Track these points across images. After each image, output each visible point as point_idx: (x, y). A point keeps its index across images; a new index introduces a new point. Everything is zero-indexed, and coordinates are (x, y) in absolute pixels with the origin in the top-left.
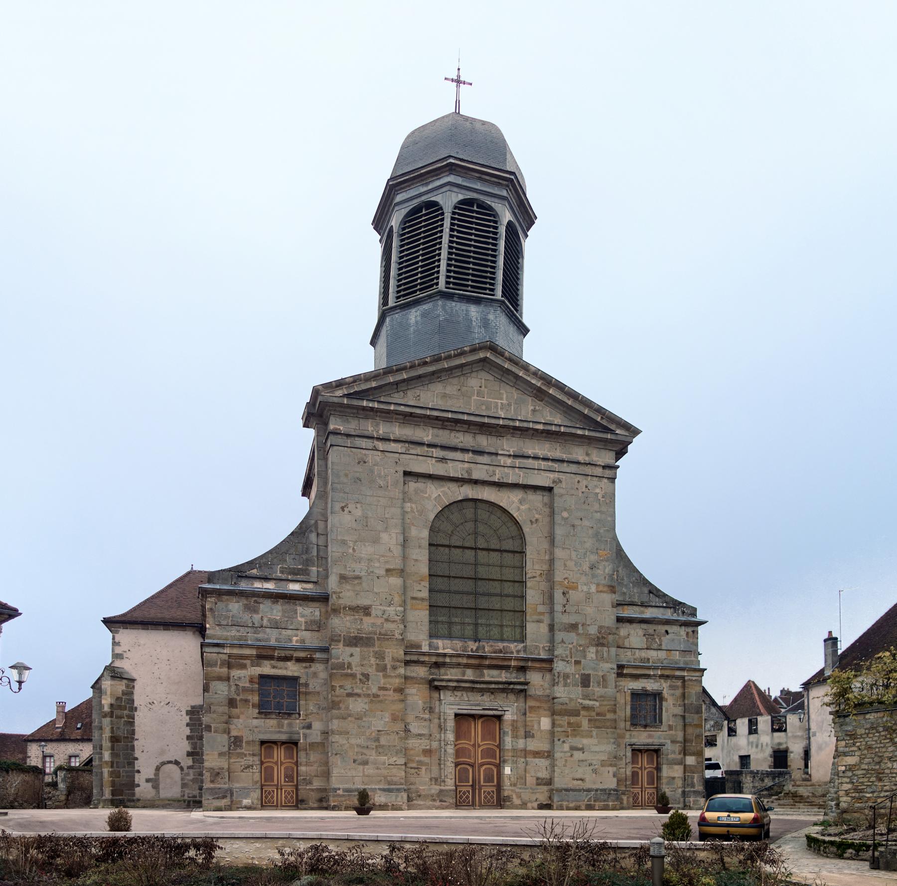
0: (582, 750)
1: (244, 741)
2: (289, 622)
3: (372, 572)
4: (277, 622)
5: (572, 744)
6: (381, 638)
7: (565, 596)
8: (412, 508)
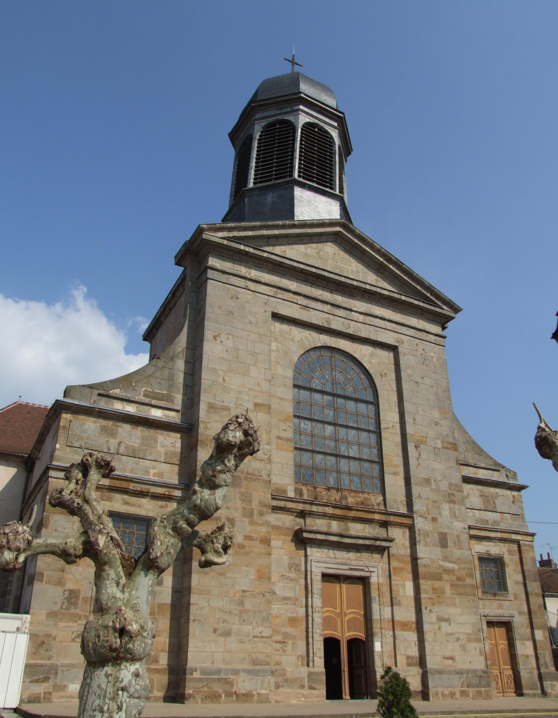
0: (448, 620)
1: (81, 597)
2: (148, 451)
3: (241, 405)
4: (134, 450)
5: (438, 614)
6: (248, 478)
7: (417, 449)
8: (277, 347)
